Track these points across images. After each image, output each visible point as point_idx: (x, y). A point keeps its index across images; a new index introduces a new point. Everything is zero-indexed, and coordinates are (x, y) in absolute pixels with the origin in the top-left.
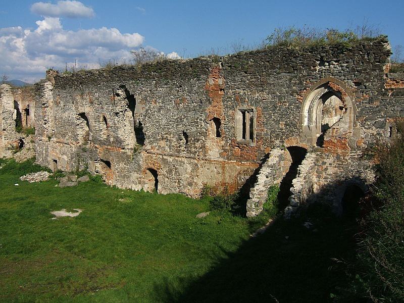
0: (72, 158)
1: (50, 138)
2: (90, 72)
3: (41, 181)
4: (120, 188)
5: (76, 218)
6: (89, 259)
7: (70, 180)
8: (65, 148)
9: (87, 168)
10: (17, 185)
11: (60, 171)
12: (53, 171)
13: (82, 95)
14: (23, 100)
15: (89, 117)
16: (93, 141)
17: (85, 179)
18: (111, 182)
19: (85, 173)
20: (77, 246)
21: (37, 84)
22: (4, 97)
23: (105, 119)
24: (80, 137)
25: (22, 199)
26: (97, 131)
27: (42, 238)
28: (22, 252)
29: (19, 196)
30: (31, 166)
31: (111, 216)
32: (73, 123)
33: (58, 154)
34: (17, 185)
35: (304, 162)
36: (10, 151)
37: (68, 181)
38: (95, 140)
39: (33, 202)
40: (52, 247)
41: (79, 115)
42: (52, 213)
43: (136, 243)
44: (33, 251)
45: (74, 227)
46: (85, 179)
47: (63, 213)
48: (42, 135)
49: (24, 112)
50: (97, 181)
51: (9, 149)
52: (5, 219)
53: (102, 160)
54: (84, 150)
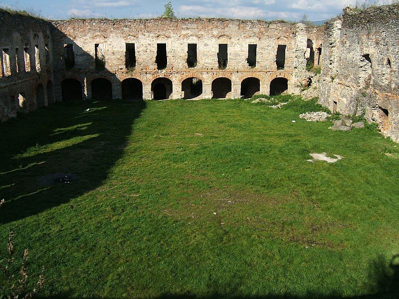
0: (351, 102)
1: (333, 79)
2: (380, 9)
3: (317, 121)
4: (394, 141)
5: (331, 164)
6: (323, 210)
7: (344, 124)
8: (346, 91)
9: (364, 114)
10: (294, 121)
11: (338, 114)
12: (332, 113)
13: (368, 34)
14: (317, 40)
15: (373, 59)
16: (373, 85)
17: (360, 125)
18: (386, 133)
19: (361, 119)
20: (317, 194)
21: (327, 23)
22: (299, 36)
23: (389, 62)
24: (361, 81)
25: (291, 136)
26: (379, 75)
27: (288, 177)
28: (265, 186)
29: (289, 133)
30: (313, 106)
31: (368, 170)
32: (356, 65)
33: (338, 95)
34: (294, 121)
35: (63, 205)
36: (298, 89)
37: (342, 125)
38: (376, 85)
39: (299, 141)
40: (294, 188)
41: (363, 56)
42: (311, 155)
43: (381, 207)
44: (275, 188)
45: (324, 173)
46: (360, 125)
47: (322, 157)
48: (326, 75)
49: (317, 51)
50: (372, 130)
51: (298, 86)
52: (267, 153)
53: (380, 108)
54: (364, 95)
